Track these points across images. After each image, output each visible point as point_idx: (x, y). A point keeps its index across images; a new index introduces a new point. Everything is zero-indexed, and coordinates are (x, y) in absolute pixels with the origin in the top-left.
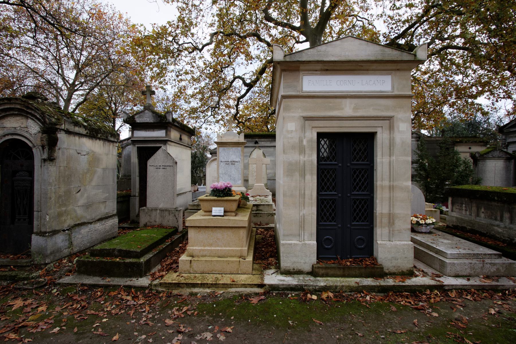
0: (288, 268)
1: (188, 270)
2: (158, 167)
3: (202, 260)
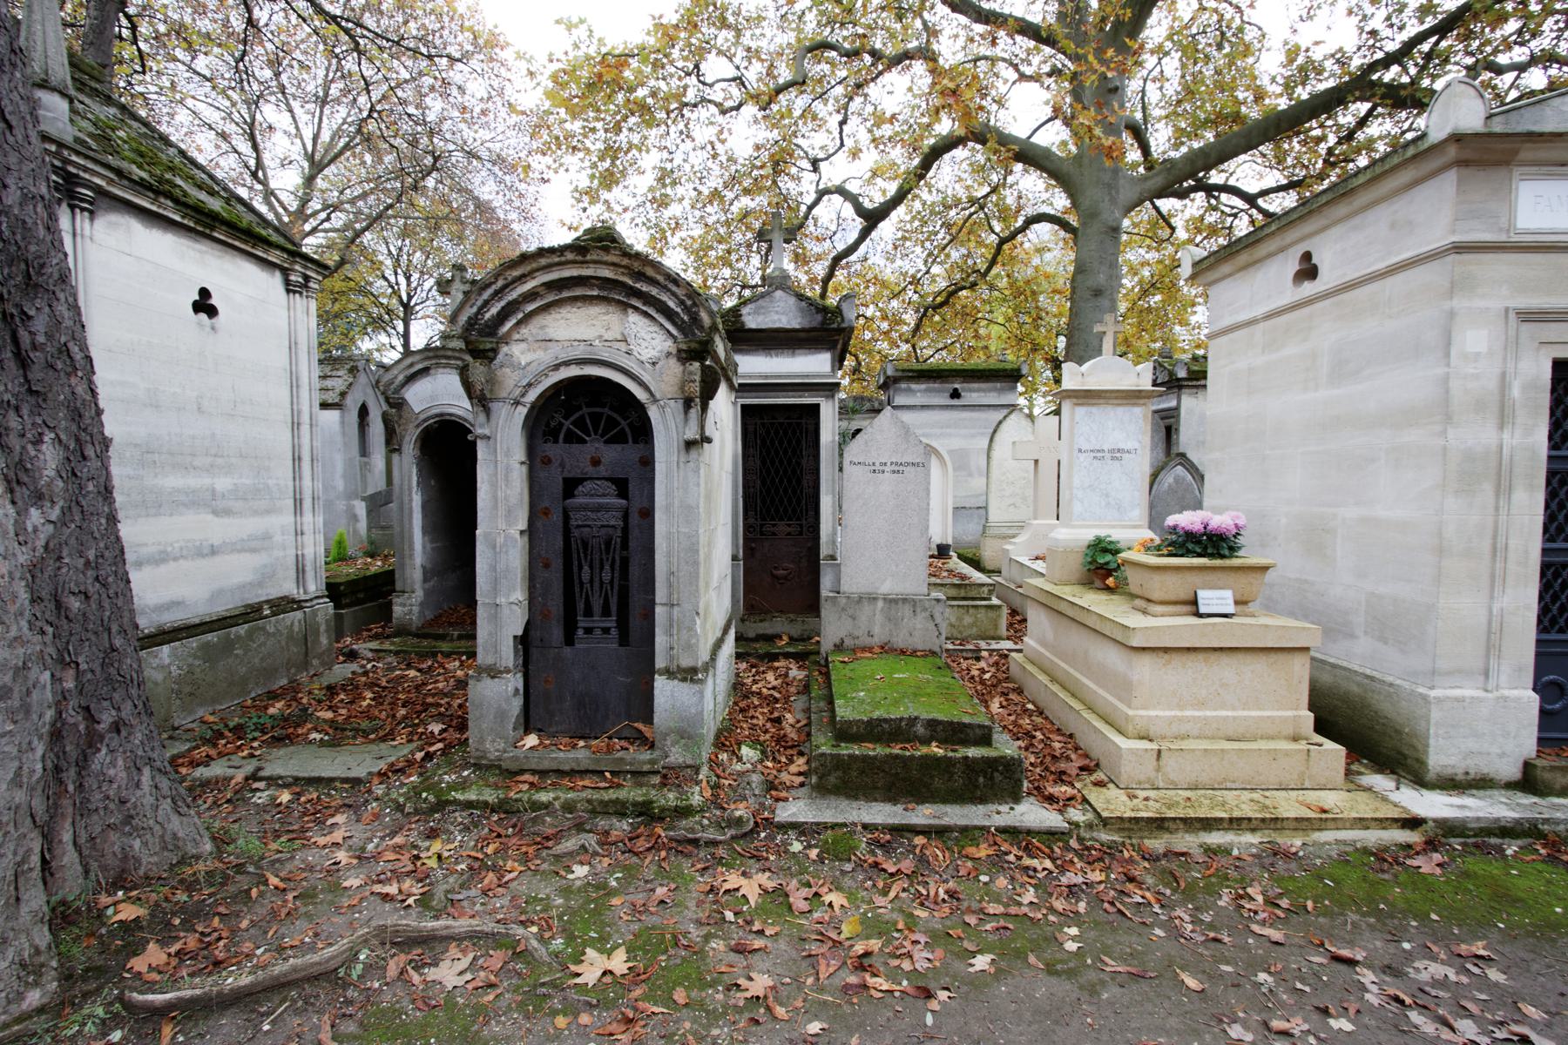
0: (1450, 771)
1: (1149, 780)
2: (877, 467)
3: (1193, 750)
